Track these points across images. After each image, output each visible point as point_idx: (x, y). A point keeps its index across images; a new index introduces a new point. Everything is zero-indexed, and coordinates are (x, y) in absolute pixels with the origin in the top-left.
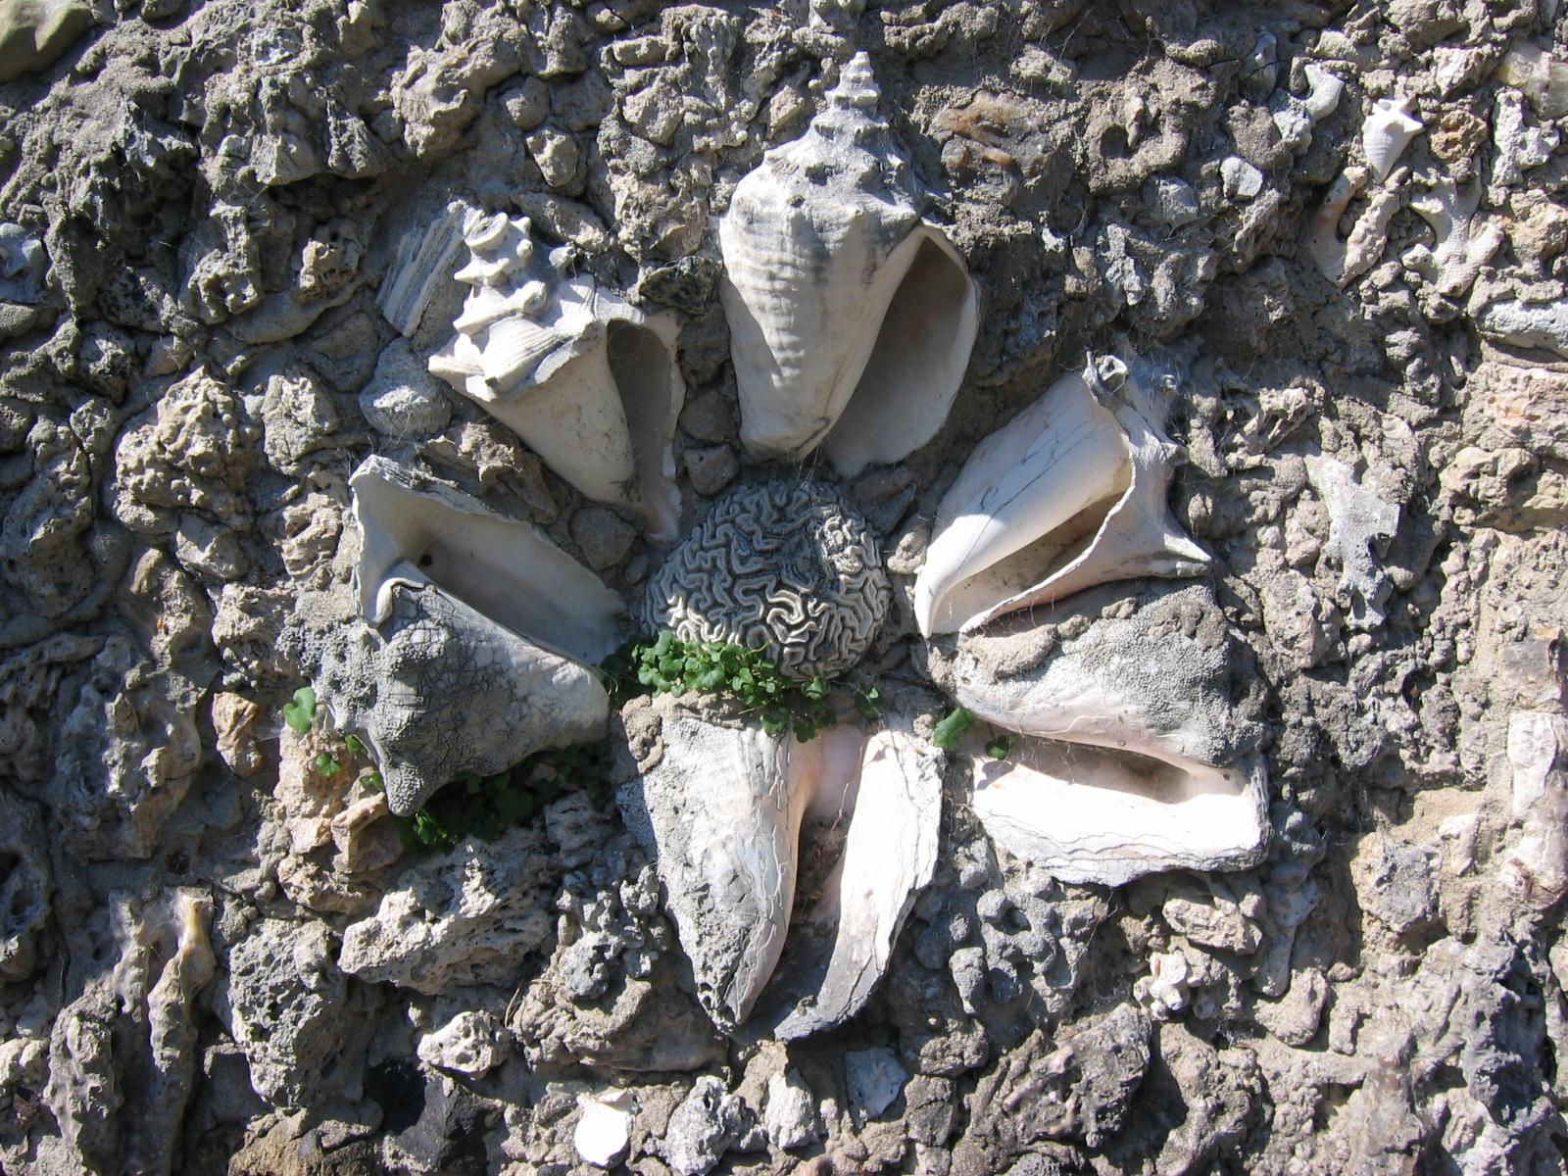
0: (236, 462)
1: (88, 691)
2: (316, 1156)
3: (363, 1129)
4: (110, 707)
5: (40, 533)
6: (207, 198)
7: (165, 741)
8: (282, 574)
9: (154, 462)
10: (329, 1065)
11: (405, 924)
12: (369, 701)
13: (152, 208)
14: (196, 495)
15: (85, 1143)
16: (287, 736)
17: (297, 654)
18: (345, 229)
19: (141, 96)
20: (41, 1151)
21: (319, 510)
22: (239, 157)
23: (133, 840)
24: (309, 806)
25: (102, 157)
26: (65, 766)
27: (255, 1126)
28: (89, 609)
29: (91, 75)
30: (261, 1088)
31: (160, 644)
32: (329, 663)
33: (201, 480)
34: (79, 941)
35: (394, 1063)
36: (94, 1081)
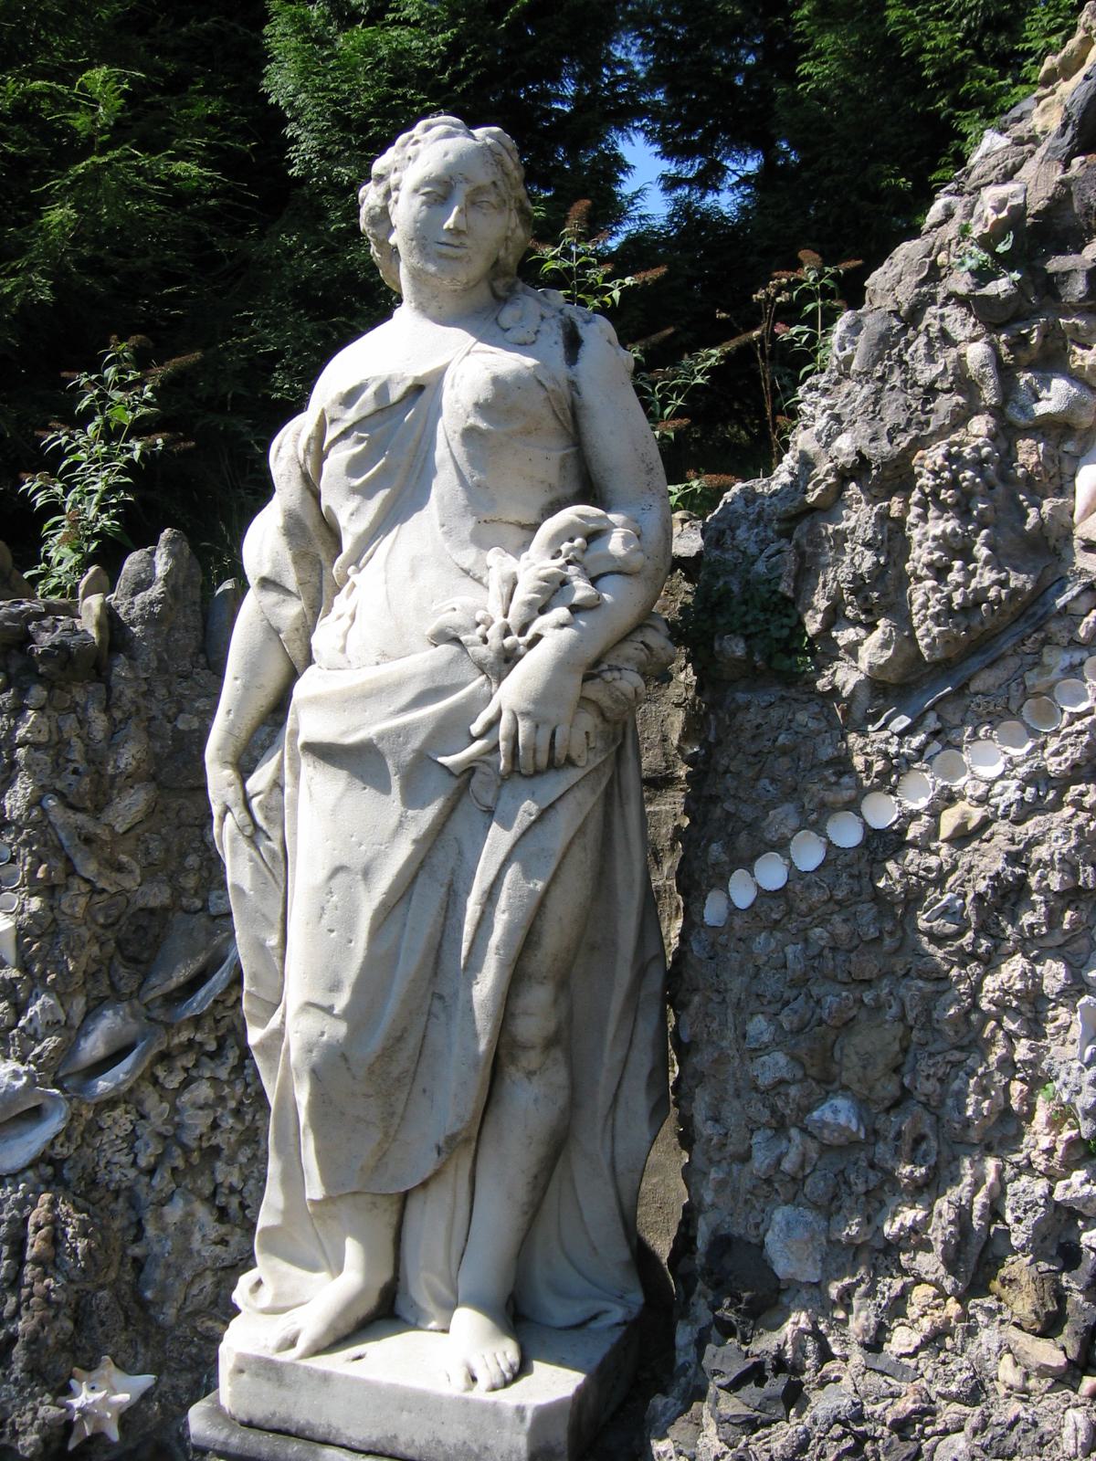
0: (1032, 992)
1: (961, 1074)
2: (1036, 1274)
3: (1055, 1268)
4: (972, 1082)
5: (952, 1011)
6: (1030, 892)
7: (991, 1097)
8: (1045, 1036)
9: (999, 989)
10: (1044, 1239)
11: (1082, 1184)
12: (1078, 1092)
13: (1009, 895)
14: (1015, 1003)
15: (944, 1253)
16: (1040, 1100)
17: (1050, 1070)
18: (1082, 906)
19: (1008, 853)
20: (918, 1257)
21: (1063, 1014)
22: (1043, 877)
23: (974, 1135)
24: (1047, 1131)
25: (992, 874)
26: (950, 1102)
27: (1010, 1259)
28: (965, 1041)
29: (988, 841)
30: (1015, 1243)
31: (993, 1059)
32: (1063, 1076)
33: (1017, 998)
34: (945, 1173)
35: (1070, 1243)
36: (951, 1228)
